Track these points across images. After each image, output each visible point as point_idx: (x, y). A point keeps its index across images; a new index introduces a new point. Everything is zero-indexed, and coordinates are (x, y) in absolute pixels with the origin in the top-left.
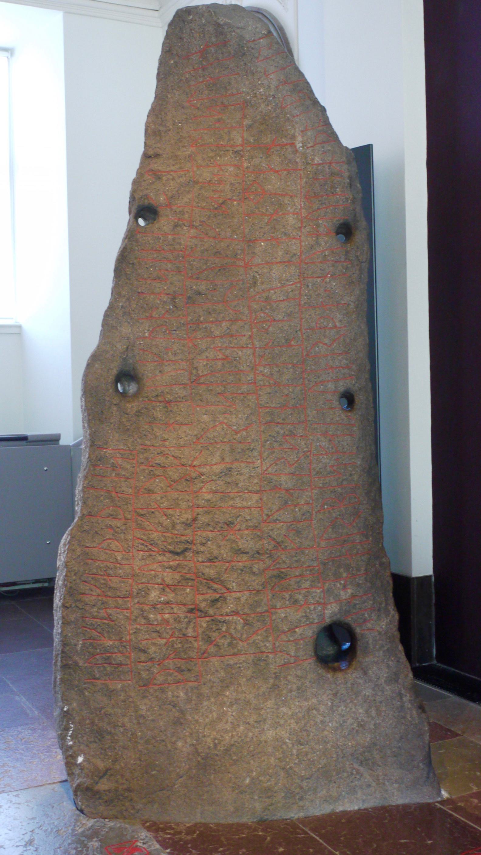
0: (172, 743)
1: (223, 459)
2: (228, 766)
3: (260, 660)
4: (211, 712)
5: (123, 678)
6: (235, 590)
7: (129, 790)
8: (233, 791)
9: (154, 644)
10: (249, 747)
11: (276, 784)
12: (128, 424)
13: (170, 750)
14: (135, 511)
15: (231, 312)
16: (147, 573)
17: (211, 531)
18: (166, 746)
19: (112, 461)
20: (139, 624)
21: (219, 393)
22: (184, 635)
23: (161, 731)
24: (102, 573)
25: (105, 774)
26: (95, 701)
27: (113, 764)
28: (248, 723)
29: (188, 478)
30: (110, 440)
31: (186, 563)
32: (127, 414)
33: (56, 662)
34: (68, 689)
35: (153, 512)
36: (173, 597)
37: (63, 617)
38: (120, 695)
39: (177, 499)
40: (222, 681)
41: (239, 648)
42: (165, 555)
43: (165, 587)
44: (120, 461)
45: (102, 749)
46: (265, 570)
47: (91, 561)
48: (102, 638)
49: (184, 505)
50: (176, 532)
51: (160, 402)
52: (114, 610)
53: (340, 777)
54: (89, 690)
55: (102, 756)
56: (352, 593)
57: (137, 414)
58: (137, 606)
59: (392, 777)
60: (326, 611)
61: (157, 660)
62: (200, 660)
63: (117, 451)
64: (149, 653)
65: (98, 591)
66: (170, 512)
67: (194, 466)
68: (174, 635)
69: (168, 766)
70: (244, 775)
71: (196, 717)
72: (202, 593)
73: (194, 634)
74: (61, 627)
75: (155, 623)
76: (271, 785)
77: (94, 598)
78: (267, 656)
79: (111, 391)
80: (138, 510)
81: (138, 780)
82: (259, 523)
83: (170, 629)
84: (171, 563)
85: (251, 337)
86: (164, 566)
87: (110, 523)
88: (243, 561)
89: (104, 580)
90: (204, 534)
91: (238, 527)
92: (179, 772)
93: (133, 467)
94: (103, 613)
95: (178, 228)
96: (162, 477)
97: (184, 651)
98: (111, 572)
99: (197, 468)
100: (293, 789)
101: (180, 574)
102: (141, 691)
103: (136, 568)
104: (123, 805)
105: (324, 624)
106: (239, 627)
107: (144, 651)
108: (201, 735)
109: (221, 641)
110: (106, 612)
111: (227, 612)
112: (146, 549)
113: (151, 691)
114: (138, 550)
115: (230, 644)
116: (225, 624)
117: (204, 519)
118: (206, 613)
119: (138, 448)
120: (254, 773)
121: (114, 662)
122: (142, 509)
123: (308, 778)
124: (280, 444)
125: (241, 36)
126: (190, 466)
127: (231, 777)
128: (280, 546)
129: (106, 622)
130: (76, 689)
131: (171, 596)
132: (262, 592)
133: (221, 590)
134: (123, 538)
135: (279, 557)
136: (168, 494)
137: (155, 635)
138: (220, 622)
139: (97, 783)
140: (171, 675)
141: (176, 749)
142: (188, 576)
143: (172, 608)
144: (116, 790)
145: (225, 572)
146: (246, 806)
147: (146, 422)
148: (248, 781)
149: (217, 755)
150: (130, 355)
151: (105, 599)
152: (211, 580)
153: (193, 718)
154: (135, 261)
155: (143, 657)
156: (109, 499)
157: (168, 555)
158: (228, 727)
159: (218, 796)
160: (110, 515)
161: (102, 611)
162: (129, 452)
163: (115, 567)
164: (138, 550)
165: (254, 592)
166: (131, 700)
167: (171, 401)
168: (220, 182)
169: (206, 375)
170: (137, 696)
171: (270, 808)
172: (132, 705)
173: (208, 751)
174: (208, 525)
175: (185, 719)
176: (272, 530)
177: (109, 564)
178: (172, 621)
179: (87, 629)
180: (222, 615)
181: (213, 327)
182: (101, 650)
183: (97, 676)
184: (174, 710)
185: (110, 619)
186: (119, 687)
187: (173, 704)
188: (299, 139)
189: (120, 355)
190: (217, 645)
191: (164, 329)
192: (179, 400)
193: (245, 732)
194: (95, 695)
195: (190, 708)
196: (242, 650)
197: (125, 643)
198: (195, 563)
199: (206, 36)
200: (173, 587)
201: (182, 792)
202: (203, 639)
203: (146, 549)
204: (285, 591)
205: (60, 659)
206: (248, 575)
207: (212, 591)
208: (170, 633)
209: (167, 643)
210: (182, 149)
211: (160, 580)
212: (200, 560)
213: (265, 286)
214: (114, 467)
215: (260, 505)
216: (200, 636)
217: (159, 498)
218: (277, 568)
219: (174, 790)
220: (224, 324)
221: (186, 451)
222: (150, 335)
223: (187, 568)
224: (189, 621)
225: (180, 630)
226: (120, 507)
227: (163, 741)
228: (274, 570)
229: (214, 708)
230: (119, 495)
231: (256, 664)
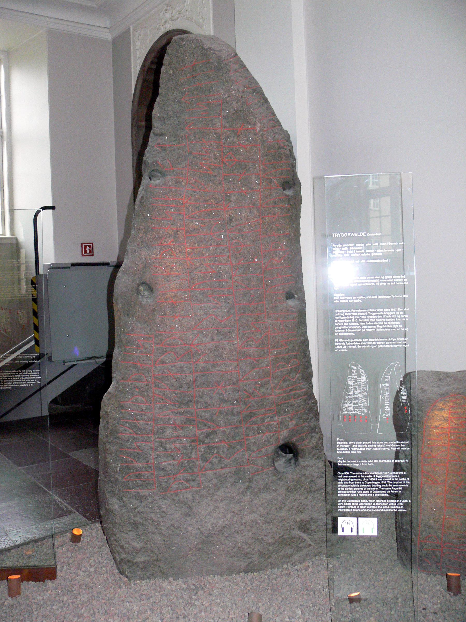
1: (213, 339)
2: (222, 540)
3: (239, 470)
5: (149, 487)
17: (206, 388)
28: (233, 512)
30: (135, 329)
36: (182, 433)
40: (215, 486)
45: (137, 535)
48: (134, 462)
49: (188, 371)
56: (296, 424)
58: (157, 440)
60: (280, 436)
64: (167, 471)
66: (179, 376)
86: (175, 412)
87: (137, 384)
88: (226, 407)
97: (190, 468)
98: (139, 418)
105: (279, 445)
106: (225, 450)
107: (163, 470)
108: (203, 523)
109: (214, 460)
113: (169, 495)
115: (220, 462)
117: (200, 380)
125: (219, 57)
135: (250, 402)
139: (135, 558)
141: (187, 532)
155: (162, 473)
160: (136, 380)
161: (134, 444)
166: (155, 502)
170: (160, 499)
172: (156, 505)
173: (209, 532)
174: (204, 384)
175: (193, 513)
180: (214, 443)
187: (184, 503)
188: (259, 125)
190: (211, 463)
199: (195, 56)
202: (202, 459)
210: (180, 131)
213: (238, 223)
221: (188, 334)
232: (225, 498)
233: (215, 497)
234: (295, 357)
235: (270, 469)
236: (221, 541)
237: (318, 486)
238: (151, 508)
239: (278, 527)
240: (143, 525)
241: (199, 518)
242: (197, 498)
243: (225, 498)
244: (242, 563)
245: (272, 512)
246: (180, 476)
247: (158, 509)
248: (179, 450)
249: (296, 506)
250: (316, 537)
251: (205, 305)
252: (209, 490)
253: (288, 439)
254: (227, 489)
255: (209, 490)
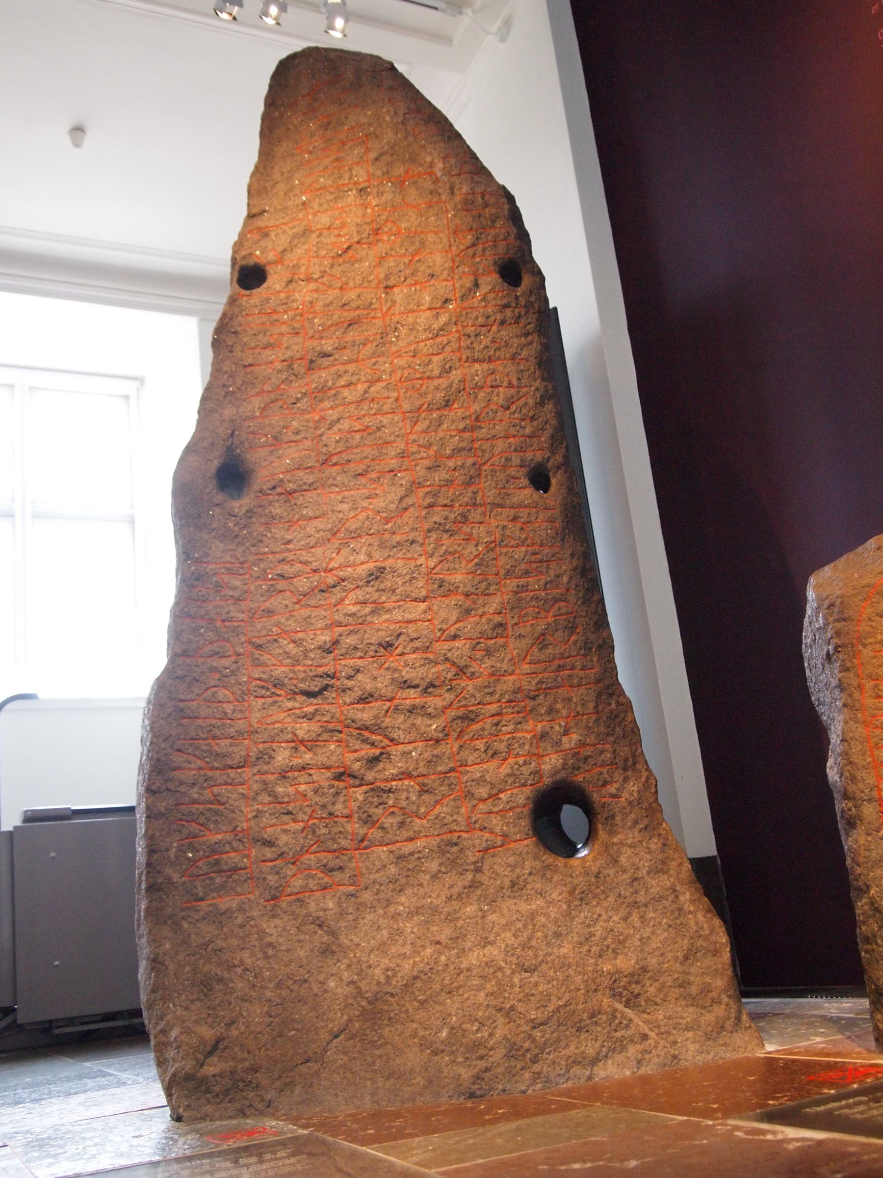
0: (320, 983)
2: (411, 1010)
4: (379, 928)
5: (239, 890)
6: (401, 740)
7: (255, 1069)
8: (422, 1051)
9: (285, 831)
10: (444, 979)
11: (491, 1035)
12: (236, 529)
13: (316, 995)
14: (250, 642)
15: (369, 371)
16: (271, 727)
18: (310, 989)
19: (215, 579)
20: (262, 804)
21: (359, 475)
22: (330, 814)
23: (301, 966)
24: (205, 736)
25: (215, 1048)
26: (197, 935)
27: (227, 1030)
28: (439, 943)
29: (323, 587)
31: (327, 707)
32: (233, 516)
33: (140, 885)
34: (157, 924)
35: (275, 640)
37: (148, 808)
38: (237, 917)
39: (309, 617)
41: (416, 829)
42: (295, 699)
43: (297, 743)
44: (226, 578)
46: (444, 709)
47: (187, 720)
48: (207, 833)
50: (310, 663)
51: (280, 494)
52: (224, 787)
53: (596, 1022)
54: (189, 919)
55: (210, 1020)
57: (248, 514)
58: (257, 778)
59: (681, 1021)
61: (291, 855)
62: (357, 852)
63: (222, 566)
65: (199, 763)
67: (331, 570)
68: (315, 815)
69: (314, 1020)
70: (438, 1023)
71: (356, 940)
72: (353, 749)
73: (346, 812)
74: (146, 823)
75: (286, 800)
76: (483, 1037)
77: (194, 772)
78: (459, 837)
79: (211, 487)
80: (253, 640)
81: (267, 1049)
82: (431, 643)
83: (308, 806)
84: (305, 709)
85: (397, 400)
87: (215, 664)
89: (208, 745)
90: (351, 662)
91: (399, 651)
92: (333, 1028)
93: (245, 584)
94: (207, 794)
95: (294, 284)
96: (288, 593)
97: (333, 839)
99: (334, 572)
100: (519, 1040)
101: (319, 724)
102: (269, 908)
103: (254, 721)
104: (246, 1099)
107: (270, 843)
108: (364, 967)
109: (388, 821)
110: (212, 792)
111: (393, 774)
112: (268, 693)
114: (256, 697)
116: (391, 795)
117: (351, 640)
118: (362, 779)
119: (251, 558)
120: (454, 1019)
121: (225, 868)
122: (259, 637)
123: (542, 1024)
124: (451, 535)
126: (325, 571)
127: (417, 1029)
128: (465, 673)
129: (212, 806)
130: (169, 922)
131: (308, 757)
132: (443, 742)
133: (381, 742)
134: (233, 681)
136: (294, 613)
137: (286, 818)
138: (384, 792)
139: (202, 1065)
140: (313, 877)
141: (326, 991)
142: (331, 726)
143: (310, 775)
144: (233, 1073)
145: (386, 716)
146: (445, 1074)
147: (262, 524)
148: (444, 1034)
149: (392, 995)
150: (236, 442)
151: (210, 774)
152: (367, 728)
153: (351, 940)
154: (239, 329)
155: (269, 853)
156: (212, 631)
157: (300, 698)
158: (408, 949)
159: (398, 1061)
160: (215, 654)
162: (238, 565)
163: (224, 725)
164: (256, 697)
165: (431, 742)
166: (252, 923)
167: (295, 491)
168: (343, 225)
169: (340, 452)
171: (487, 1075)
173: (376, 988)
175: (340, 945)
176: (450, 650)
177: (214, 722)
178: (310, 794)
179: (184, 823)
180: (386, 780)
181: (346, 393)
182: (205, 852)
183: (201, 894)
184: (320, 932)
185: (218, 801)
186: (234, 905)
189: (222, 443)
190: (383, 828)
191: (280, 403)
192: (305, 487)
193: (435, 956)
194: (198, 925)
195: (345, 927)
196: (421, 832)
197: (241, 835)
198: (340, 706)
200: (310, 743)
201: (340, 1061)
202: (360, 818)
203: (268, 693)
204: (477, 739)
205: (144, 879)
206: (420, 718)
207: (368, 746)
208: (309, 812)
209: (304, 828)
211: (290, 736)
212: (348, 701)
214: (219, 587)
215: (430, 617)
216: (356, 816)
217: (283, 620)
218: (464, 706)
219: (326, 1060)
220: (359, 386)
221: (319, 551)
222: (261, 413)
223: (329, 715)
224: (337, 793)
225: (324, 806)
226: (228, 641)
227: (306, 981)
228: (458, 708)
229: (383, 922)
230: (227, 624)
231: (444, 853)
232: (417, 911)
233: (392, 909)
234: (562, 599)
235: (525, 842)
236: (406, 1011)
237: (652, 891)
238: (242, 938)
239: (555, 983)
240: (221, 980)
241: (355, 956)
242: (351, 911)
243: (417, 911)
244: (462, 1071)
245: (534, 943)
246: (310, 859)
247: (257, 940)
248: (305, 796)
249: (598, 934)
250: (661, 1017)
251: (352, 493)
252: (378, 892)
253: (562, 775)
254: (421, 890)
255: (378, 892)
